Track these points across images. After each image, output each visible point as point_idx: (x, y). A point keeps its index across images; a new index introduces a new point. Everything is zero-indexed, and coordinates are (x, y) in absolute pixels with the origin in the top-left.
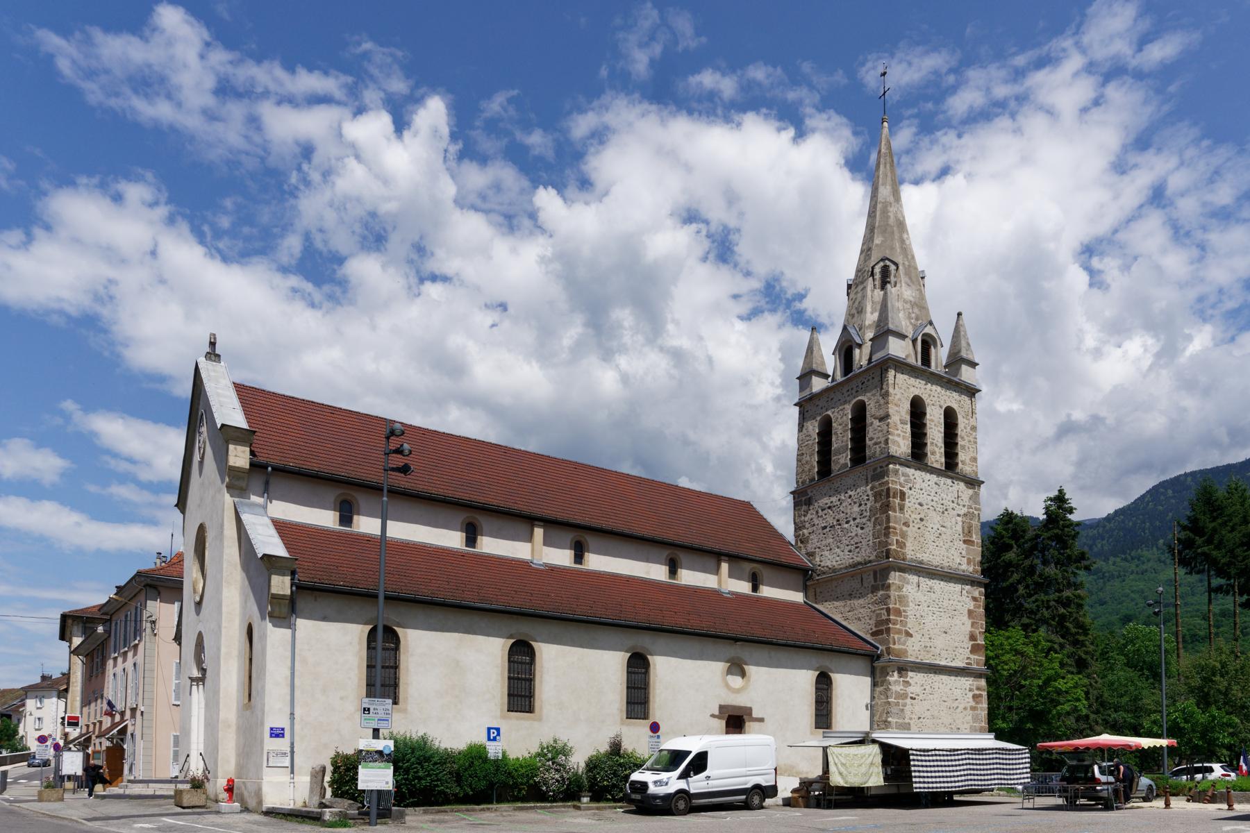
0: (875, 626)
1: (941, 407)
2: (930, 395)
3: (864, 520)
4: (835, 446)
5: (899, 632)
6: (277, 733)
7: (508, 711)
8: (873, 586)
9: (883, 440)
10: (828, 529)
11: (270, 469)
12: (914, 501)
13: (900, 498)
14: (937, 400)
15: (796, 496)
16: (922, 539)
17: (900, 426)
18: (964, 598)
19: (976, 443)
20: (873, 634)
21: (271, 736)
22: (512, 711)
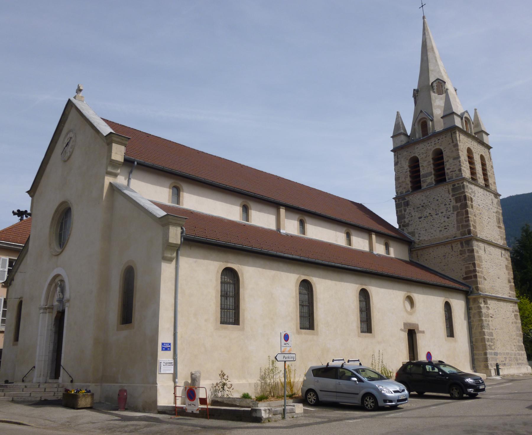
1: (479, 154)
2: (474, 148)
3: (449, 213)
4: (422, 172)
5: (481, 277)
6: (166, 348)
8: (461, 251)
9: (457, 169)
10: (423, 219)
11: (136, 163)
12: (476, 203)
13: (471, 201)
14: (478, 150)
15: (397, 200)
16: (482, 224)
17: (465, 162)
18: (503, 258)
19: (494, 174)
20: (465, 279)
21: (162, 350)
22: (303, 329)
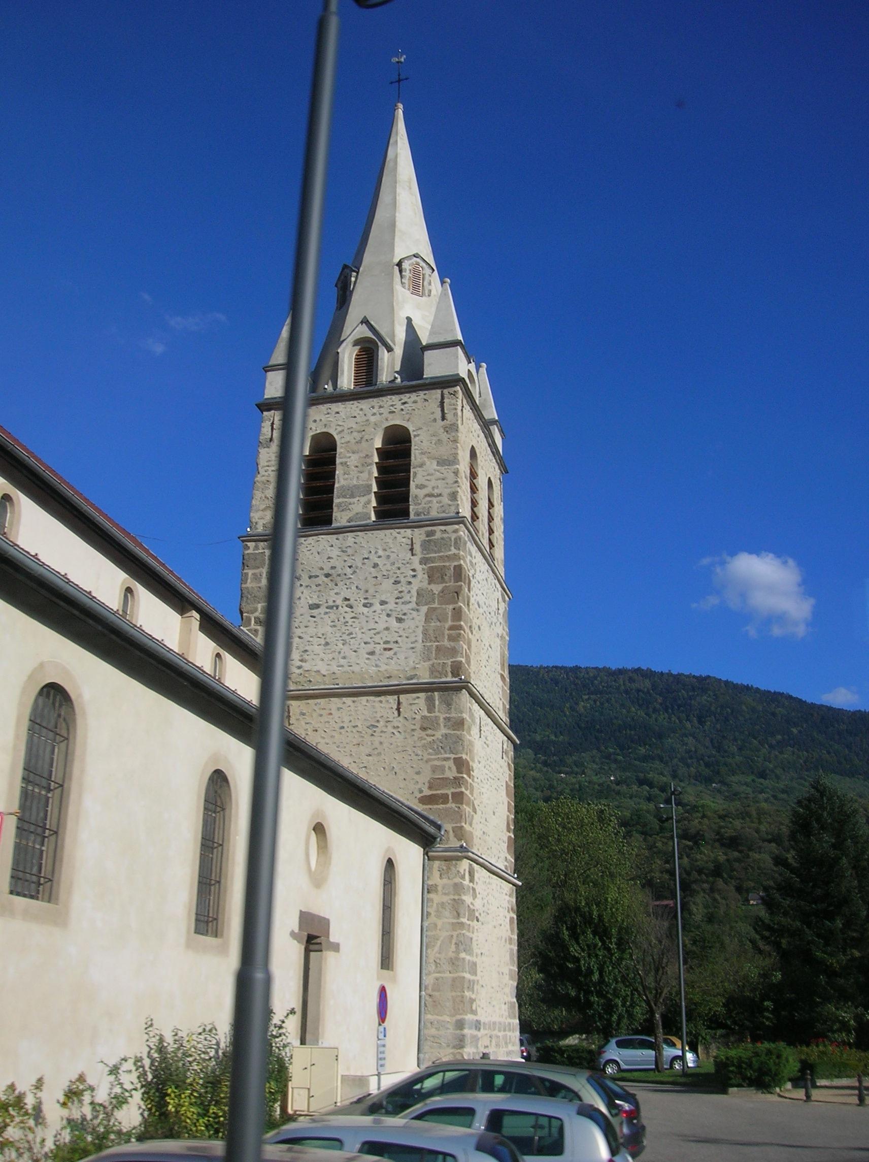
0: (430, 788)
3: (405, 608)
7: (195, 933)
10: (323, 610)
20: (425, 800)
22: (18, 894)
